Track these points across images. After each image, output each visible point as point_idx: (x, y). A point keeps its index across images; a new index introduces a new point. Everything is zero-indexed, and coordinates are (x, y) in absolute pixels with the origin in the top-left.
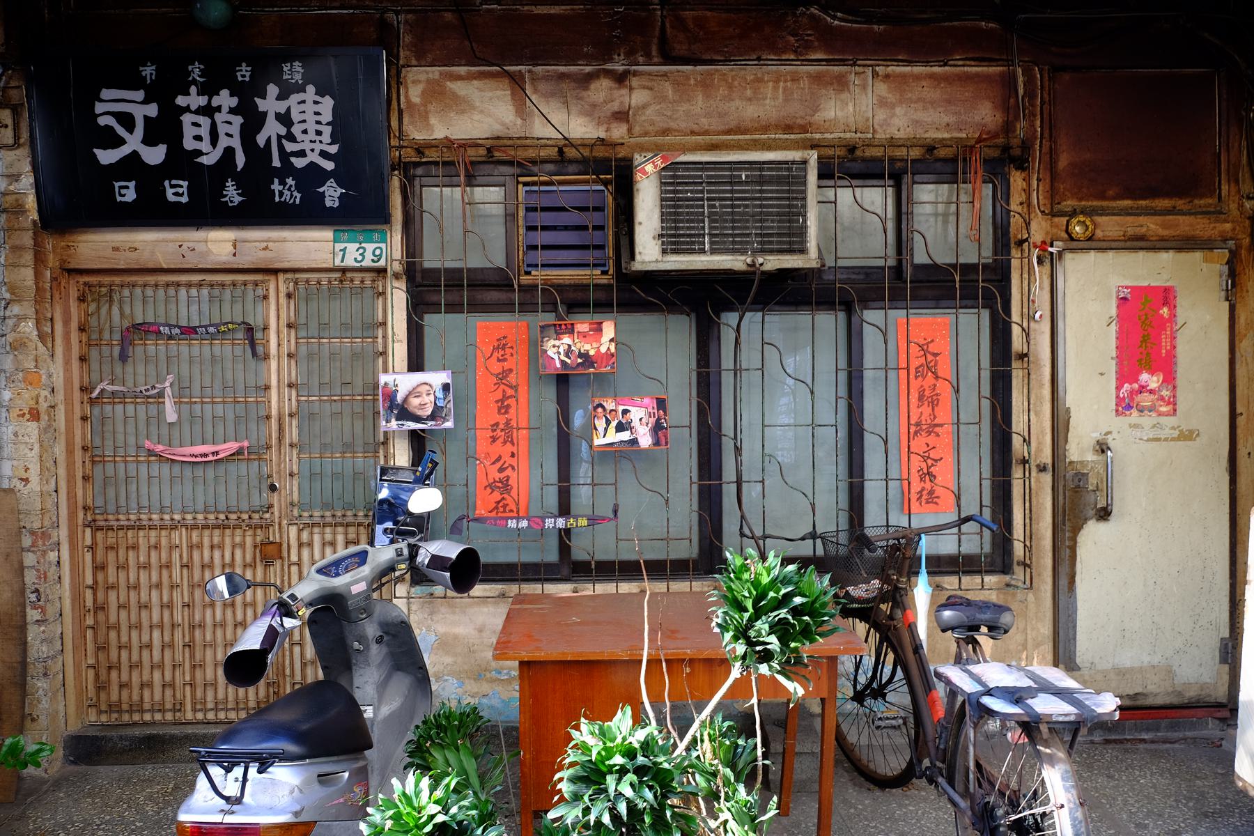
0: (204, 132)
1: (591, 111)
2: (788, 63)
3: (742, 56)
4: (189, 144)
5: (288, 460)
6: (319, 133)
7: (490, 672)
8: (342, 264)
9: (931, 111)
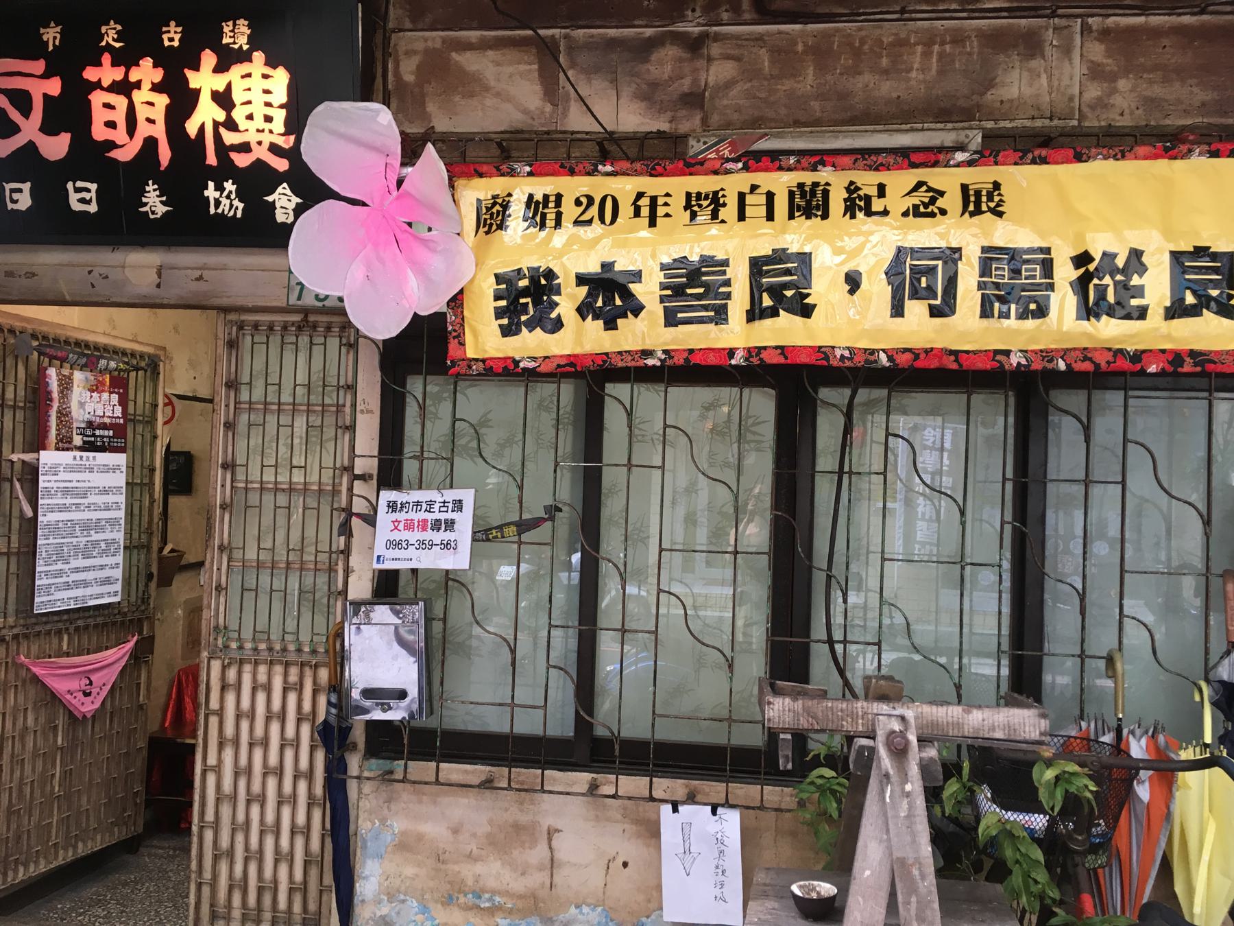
0: (120, 116)
1: (649, 95)
2: (947, 15)
3: (877, 7)
4: (99, 132)
5: (215, 568)
6: (268, 119)
7: (465, 896)
8: (299, 303)
9: (1177, 85)
